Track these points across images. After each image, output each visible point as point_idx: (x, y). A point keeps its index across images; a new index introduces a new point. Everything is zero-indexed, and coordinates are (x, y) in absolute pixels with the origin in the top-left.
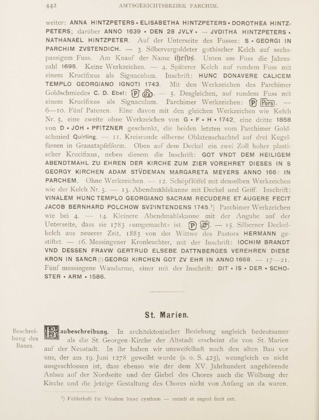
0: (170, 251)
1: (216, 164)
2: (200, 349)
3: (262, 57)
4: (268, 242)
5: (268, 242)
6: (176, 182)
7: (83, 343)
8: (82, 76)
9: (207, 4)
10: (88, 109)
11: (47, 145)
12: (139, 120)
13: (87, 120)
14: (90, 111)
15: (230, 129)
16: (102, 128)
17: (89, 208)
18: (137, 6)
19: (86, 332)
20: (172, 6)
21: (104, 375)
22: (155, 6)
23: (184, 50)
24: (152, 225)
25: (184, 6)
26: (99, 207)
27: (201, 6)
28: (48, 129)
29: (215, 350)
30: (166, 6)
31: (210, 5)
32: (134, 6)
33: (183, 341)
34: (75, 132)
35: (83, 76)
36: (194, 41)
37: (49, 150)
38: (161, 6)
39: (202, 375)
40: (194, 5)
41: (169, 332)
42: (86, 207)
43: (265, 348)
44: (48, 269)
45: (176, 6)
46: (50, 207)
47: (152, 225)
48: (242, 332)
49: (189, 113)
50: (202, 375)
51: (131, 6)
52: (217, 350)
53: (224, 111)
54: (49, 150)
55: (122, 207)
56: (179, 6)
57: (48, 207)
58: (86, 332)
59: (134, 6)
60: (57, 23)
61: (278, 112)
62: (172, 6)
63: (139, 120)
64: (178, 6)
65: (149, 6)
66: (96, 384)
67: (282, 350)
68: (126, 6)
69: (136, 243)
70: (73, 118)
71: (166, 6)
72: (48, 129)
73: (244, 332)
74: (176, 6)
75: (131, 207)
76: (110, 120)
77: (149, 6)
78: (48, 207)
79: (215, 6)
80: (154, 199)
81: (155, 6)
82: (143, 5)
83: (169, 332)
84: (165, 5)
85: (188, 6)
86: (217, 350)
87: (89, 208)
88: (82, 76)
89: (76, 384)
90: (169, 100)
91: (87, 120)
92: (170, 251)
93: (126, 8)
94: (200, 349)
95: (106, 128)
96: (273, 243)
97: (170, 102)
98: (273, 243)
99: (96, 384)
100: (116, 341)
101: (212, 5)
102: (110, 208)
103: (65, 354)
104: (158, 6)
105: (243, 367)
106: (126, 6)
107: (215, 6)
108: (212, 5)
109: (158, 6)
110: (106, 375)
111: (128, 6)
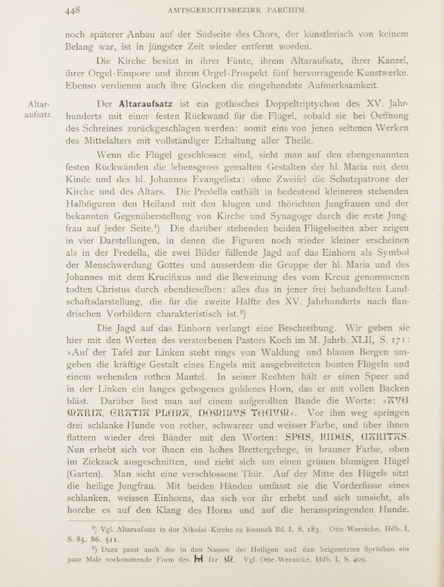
6: (91, 129)
7: (190, 305)
8: (167, 278)
12: (339, 86)
13: (209, 302)
15: (299, 129)
18: (193, 10)
21: (293, 47)
22: (218, 10)
25: (258, 10)
27: (282, 10)
30: (233, 10)
31: (295, 9)
33: (285, 168)
35: (168, 278)
36: (344, 229)
37: (71, 296)
38: (226, 10)
39: (332, 105)
41: (94, 426)
43: (363, 350)
44: (237, 242)
45: (247, 10)
50: (332, 105)
51: (185, 10)
53: (113, 314)
54: (71, 296)
56: (252, 10)
60: (146, 229)
63: (339, 86)
66: (314, 129)
67: (164, 427)
68: (176, 10)
71: (233, 10)
74: (247, 10)
76: (254, 180)
79: (302, 10)
81: (218, 10)
82: (201, 10)
83: (94, 426)
84: (232, 10)
88: (167, 278)
90: (239, 338)
97: (241, 341)
99: (314, 129)
100: (373, 353)
101: (298, 9)
103: (169, 335)
104: (222, 10)
106: (176, 10)
107: (302, 10)
108: (298, 9)
109: (222, 10)
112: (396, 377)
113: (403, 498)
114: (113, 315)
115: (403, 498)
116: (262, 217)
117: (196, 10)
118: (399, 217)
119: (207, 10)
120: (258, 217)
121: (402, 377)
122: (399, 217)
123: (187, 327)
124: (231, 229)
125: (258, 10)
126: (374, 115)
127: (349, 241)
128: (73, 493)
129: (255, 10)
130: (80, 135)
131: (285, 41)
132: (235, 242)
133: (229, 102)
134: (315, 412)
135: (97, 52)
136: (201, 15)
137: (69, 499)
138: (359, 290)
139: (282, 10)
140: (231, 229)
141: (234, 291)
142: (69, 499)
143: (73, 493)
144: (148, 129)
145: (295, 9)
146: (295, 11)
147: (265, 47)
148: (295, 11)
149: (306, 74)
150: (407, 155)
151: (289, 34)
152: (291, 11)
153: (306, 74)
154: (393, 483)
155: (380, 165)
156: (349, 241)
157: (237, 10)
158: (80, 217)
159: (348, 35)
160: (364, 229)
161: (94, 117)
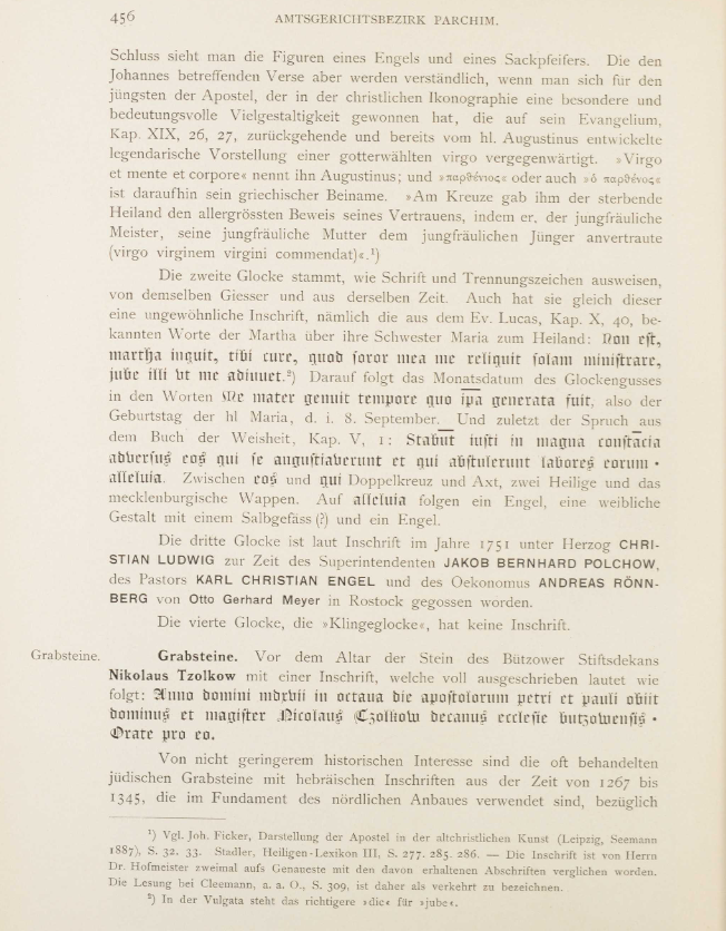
6: (387, 338)
10: (144, 576)
14: (147, 580)
17: (542, 566)
22: (357, 19)
25: (420, 21)
26: (566, 564)
27: (459, 21)
28: (163, 602)
30: (380, 19)
31: (479, 20)
32: (309, 19)
34: (320, 86)
42: (536, 564)
45: (402, 19)
46: (456, 563)
48: (360, 318)
49: (575, 305)
51: (302, 19)
55: (617, 564)
57: (451, 564)
59: (309, 19)
62: (395, 19)
65: (343, 19)
68: (289, 19)
69: (458, 198)
70: (557, 117)
71: (380, 19)
72: (163, 602)
75: (637, 564)
77: (343, 19)
78: (451, 564)
79: (490, 21)
81: (357, 19)
84: (378, 19)
85: (429, 20)
87: (542, 566)
91: (518, 483)
93: (289, 23)
96: (547, 564)
98: (547, 564)
101: (484, 20)
102: (590, 567)
104: (363, 20)
106: (289, 19)
107: (490, 21)
108: (484, 20)
111: (296, 19)
112: (641, 102)
113: (613, 403)
114: (265, 659)
115: (613, 403)
117: (320, 17)
120: (292, 297)
121: (649, 101)
125: (420, 21)
126: (457, 582)
129: (416, 20)
130: (127, 874)
131: (324, 845)
132: (217, 799)
133: (383, 94)
134: (221, 152)
135: (161, 526)
136: (328, 12)
138: (490, 218)
139: (459, 21)
144: (473, 80)
145: (479, 20)
148: (479, 22)
149: (496, 802)
151: (331, 838)
153: (496, 802)
154: (483, 622)
155: (276, 777)
157: (386, 19)
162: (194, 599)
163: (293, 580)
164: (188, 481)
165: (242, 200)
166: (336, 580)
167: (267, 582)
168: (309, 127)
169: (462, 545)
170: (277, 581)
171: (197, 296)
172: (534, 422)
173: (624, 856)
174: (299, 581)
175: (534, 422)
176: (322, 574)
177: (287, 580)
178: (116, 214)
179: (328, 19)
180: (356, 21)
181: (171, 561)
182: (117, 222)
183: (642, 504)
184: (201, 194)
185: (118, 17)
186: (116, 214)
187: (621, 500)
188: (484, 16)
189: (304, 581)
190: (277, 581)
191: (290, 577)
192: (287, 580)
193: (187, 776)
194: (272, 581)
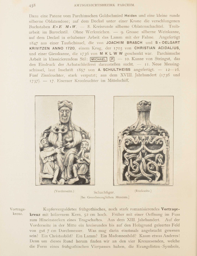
0: (103, 225)
1: (110, 43)
2: (95, 220)
3: (151, 246)
4: (129, 43)
5: (129, 43)
9: (128, 4)
11: (31, 27)
16: (40, 48)
19: (34, 215)
20: (107, 5)
21: (36, 226)
23: (107, 16)
24: (101, 231)
25: (114, 5)
27: (124, 5)
29: (101, 215)
31: (130, 5)
37: (32, 30)
38: (100, 5)
40: (120, 4)
47: (101, 231)
52: (102, 215)
58: (34, 215)
61: (75, 215)
62: (107, 5)
64: (110, 5)
67: (99, 43)
68: (78, 5)
73: (116, 209)
79: (133, 5)
80: (55, 49)
85: (116, 5)
86: (102, 215)
89: (144, 16)
92: (103, 225)
93: (78, 7)
94: (95, 220)
95: (42, 48)
96: (132, 43)
98: (132, 43)
100: (61, 210)
101: (131, 5)
104: (98, 5)
105: (158, 220)
106: (78, 5)
107: (133, 5)
109: (98, 5)
110: (38, 226)
111: (80, 5)
116: (144, 16)
118: (168, 21)
119: (91, 5)
122: (168, 21)
123: (45, 75)
124: (100, 231)
125: (114, 5)
127: (81, 38)
128: (32, 68)
129: (112, 5)
137: (30, 70)
139: (124, 5)
140: (100, 231)
141: (159, 48)
142: (30, 70)
143: (32, 68)
146: (130, 5)
147: (125, 27)
150: (178, 16)
152: (128, 5)
156: (81, 38)
158: (170, 32)
159: (81, 65)
160: (75, 38)
161: (173, 37)
162: (62, 48)
163: (148, 48)
164: (42, 76)
165: (126, 55)
166: (47, 48)
167: (141, 49)
168: (139, 73)
169: (163, 54)
170: (144, 48)
171: (78, 38)
172: (94, 75)
173: (171, 225)
174: (150, 48)
175: (94, 75)
176: (51, 47)
177: (147, 48)
178: (41, 221)
179: (89, 5)
180: (128, 5)
181: (175, 48)
182: (31, 24)
183: (157, 231)
184: (127, 241)
185: (31, 5)
186: (134, 226)
187: (176, 26)
188: (131, 4)
189: (151, 48)
190: (144, 48)
191: (41, 47)
192: (147, 48)
193: (101, 15)
194: (143, 48)
